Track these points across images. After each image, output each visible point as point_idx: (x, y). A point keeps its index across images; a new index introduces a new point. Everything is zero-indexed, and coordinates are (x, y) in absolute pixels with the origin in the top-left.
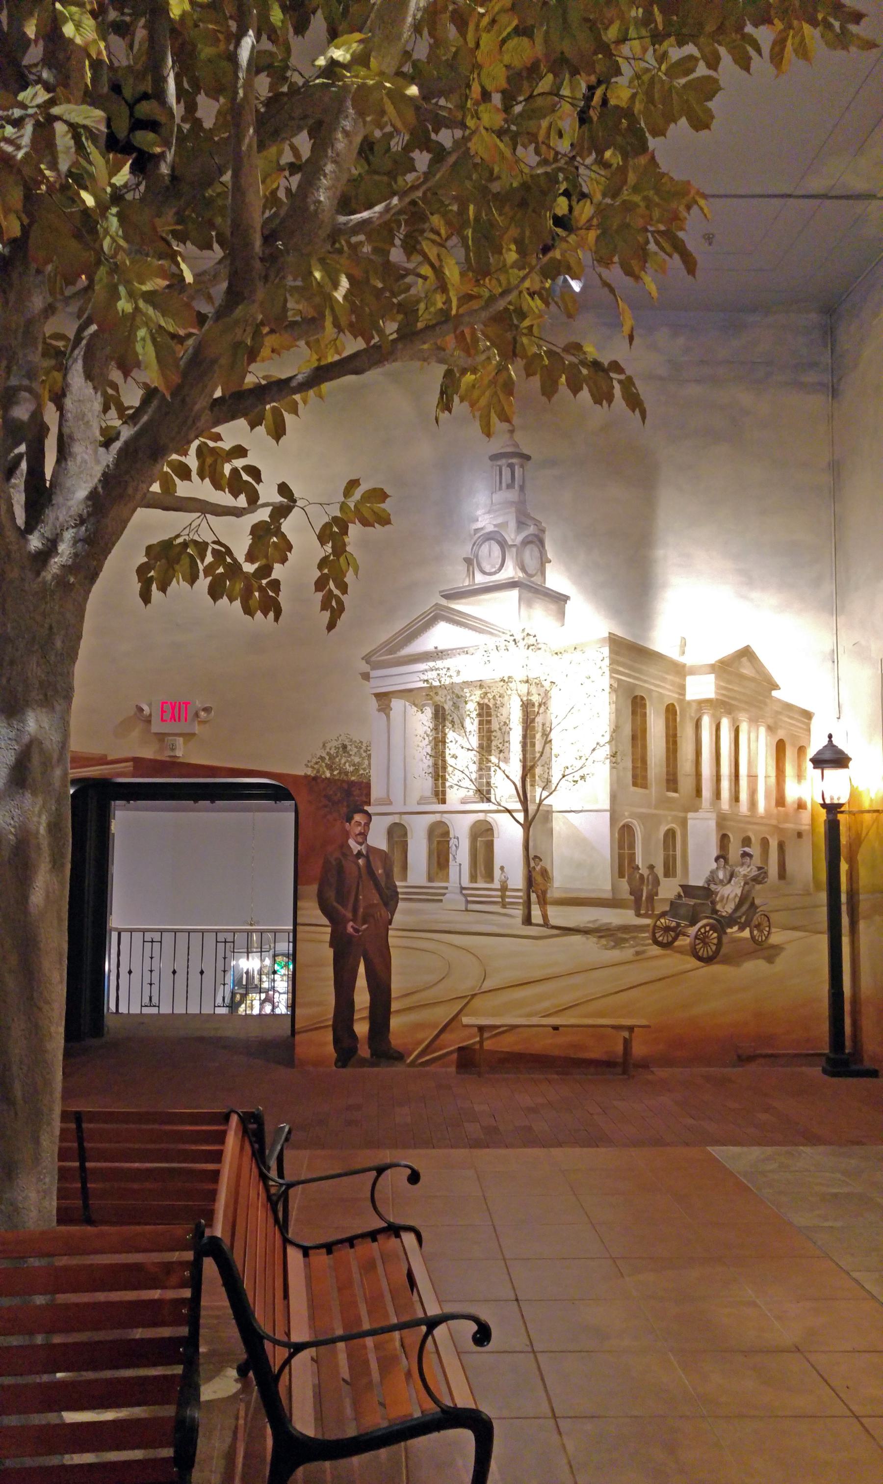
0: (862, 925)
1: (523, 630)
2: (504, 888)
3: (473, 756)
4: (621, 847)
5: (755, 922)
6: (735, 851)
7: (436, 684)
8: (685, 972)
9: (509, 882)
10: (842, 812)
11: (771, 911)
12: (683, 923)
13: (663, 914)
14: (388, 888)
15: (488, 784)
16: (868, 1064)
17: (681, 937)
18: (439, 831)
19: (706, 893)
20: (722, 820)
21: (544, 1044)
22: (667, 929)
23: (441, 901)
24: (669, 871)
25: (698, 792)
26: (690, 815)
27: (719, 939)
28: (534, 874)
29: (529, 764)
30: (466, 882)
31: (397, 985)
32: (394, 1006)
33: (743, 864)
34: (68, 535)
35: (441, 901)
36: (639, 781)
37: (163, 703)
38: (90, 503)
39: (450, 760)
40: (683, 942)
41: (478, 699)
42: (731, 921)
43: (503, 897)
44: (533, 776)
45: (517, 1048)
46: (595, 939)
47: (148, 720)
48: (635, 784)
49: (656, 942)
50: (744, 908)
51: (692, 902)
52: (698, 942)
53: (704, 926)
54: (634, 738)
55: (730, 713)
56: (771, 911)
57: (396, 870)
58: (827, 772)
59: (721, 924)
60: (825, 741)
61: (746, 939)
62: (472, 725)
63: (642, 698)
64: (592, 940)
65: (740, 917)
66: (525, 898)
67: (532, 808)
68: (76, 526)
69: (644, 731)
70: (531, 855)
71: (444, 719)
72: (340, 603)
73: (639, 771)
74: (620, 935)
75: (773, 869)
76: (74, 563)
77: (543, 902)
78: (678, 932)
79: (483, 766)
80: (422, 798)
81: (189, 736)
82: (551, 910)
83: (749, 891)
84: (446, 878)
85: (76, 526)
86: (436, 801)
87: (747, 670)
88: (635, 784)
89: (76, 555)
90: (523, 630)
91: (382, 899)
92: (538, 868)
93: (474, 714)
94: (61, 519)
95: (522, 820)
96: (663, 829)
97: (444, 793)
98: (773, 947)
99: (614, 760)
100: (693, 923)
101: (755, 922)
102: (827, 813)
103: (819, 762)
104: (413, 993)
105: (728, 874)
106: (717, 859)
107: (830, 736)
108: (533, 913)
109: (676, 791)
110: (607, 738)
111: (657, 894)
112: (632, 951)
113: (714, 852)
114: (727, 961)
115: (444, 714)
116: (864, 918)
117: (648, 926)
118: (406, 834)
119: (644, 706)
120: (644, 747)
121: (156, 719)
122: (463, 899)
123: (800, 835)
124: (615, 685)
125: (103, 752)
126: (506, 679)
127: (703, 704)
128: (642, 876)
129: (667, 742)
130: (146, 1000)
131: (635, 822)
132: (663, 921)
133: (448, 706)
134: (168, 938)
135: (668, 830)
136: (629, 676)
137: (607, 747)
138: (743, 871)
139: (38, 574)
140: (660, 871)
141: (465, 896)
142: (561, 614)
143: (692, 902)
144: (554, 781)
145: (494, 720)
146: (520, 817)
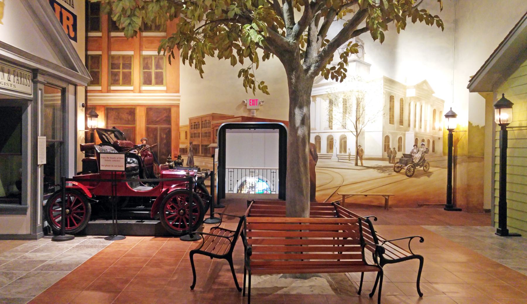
0: (458, 166)
1: (357, 75)
2: (350, 155)
3: (341, 115)
4: (385, 142)
5: (425, 165)
6: (419, 144)
7: (330, 92)
8: (403, 180)
9: (351, 153)
10: (454, 131)
11: (430, 162)
12: (403, 165)
13: (397, 163)
14: (315, 155)
15: (345, 123)
16: (458, 207)
17: (402, 170)
18: (331, 138)
19: (410, 156)
20: (416, 134)
21: (361, 201)
22: (398, 167)
23: (331, 159)
24: (400, 149)
25: (409, 125)
26: (407, 132)
27: (414, 170)
28: (359, 151)
29: (358, 117)
30: (338, 153)
31: (318, 183)
32: (317, 189)
33: (422, 148)
34: (313, 65)
35: (331, 159)
36: (392, 122)
37: (250, 100)
38: (319, 58)
39: (333, 116)
40: (403, 171)
41: (343, 97)
42: (418, 164)
43: (349, 158)
44: (359, 121)
45: (353, 202)
46: (377, 170)
47: (246, 105)
48: (390, 123)
49: (395, 171)
50: (422, 161)
51: (406, 159)
52: (407, 171)
53: (409, 166)
54: (390, 109)
55: (419, 101)
56: (430, 162)
57: (317, 150)
58: (450, 119)
59: (415, 165)
60: (449, 110)
61: (422, 170)
62: (341, 105)
63: (393, 96)
64: (376, 170)
65: (420, 163)
66: (356, 158)
67: (359, 131)
68: (316, 63)
69: (393, 107)
70: (358, 145)
71: (332, 104)
72: (344, 74)
73: (391, 119)
74: (384, 169)
75: (431, 149)
76: (314, 72)
77: (361, 159)
78: (401, 168)
79: (344, 118)
80: (325, 128)
81: (257, 110)
82: (364, 162)
83: (423, 156)
84: (332, 152)
85: (316, 63)
86: (329, 129)
87: (425, 87)
88: (390, 123)
89: (315, 70)
90: (357, 75)
91: (313, 158)
92: (360, 149)
93: (341, 102)
94: (311, 61)
95: (355, 135)
96: (398, 137)
97: (332, 126)
98: (430, 172)
99: (384, 115)
100: (406, 165)
101: (425, 165)
102: (449, 132)
103: (447, 116)
104: (322, 186)
105: (417, 150)
106: (414, 146)
107: (451, 108)
108: (358, 162)
109: (402, 125)
110: (382, 109)
111: (396, 157)
112: (387, 174)
113: (414, 144)
114: (416, 176)
115: (332, 102)
116: (459, 164)
117: (393, 166)
118: (320, 139)
119: (393, 99)
120: (393, 112)
121: (248, 105)
122: (337, 158)
123: (439, 139)
124: (385, 92)
125: (233, 115)
126: (351, 91)
127: (411, 98)
128: (391, 151)
129: (400, 110)
130: (230, 189)
131: (390, 135)
132: (397, 164)
133: (334, 100)
134: (236, 171)
135: (400, 137)
136: (389, 89)
137: (382, 111)
138: (422, 149)
139: (306, 75)
140: (397, 149)
141: (338, 157)
142: (369, 70)
143: (406, 159)
144: (365, 122)
145: (347, 103)
146: (355, 133)
